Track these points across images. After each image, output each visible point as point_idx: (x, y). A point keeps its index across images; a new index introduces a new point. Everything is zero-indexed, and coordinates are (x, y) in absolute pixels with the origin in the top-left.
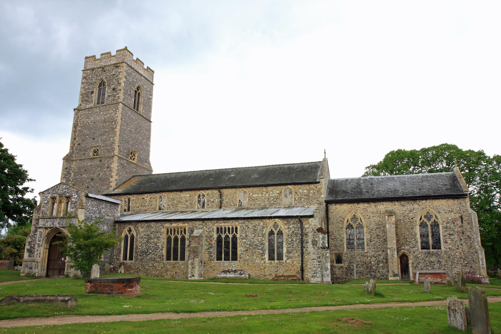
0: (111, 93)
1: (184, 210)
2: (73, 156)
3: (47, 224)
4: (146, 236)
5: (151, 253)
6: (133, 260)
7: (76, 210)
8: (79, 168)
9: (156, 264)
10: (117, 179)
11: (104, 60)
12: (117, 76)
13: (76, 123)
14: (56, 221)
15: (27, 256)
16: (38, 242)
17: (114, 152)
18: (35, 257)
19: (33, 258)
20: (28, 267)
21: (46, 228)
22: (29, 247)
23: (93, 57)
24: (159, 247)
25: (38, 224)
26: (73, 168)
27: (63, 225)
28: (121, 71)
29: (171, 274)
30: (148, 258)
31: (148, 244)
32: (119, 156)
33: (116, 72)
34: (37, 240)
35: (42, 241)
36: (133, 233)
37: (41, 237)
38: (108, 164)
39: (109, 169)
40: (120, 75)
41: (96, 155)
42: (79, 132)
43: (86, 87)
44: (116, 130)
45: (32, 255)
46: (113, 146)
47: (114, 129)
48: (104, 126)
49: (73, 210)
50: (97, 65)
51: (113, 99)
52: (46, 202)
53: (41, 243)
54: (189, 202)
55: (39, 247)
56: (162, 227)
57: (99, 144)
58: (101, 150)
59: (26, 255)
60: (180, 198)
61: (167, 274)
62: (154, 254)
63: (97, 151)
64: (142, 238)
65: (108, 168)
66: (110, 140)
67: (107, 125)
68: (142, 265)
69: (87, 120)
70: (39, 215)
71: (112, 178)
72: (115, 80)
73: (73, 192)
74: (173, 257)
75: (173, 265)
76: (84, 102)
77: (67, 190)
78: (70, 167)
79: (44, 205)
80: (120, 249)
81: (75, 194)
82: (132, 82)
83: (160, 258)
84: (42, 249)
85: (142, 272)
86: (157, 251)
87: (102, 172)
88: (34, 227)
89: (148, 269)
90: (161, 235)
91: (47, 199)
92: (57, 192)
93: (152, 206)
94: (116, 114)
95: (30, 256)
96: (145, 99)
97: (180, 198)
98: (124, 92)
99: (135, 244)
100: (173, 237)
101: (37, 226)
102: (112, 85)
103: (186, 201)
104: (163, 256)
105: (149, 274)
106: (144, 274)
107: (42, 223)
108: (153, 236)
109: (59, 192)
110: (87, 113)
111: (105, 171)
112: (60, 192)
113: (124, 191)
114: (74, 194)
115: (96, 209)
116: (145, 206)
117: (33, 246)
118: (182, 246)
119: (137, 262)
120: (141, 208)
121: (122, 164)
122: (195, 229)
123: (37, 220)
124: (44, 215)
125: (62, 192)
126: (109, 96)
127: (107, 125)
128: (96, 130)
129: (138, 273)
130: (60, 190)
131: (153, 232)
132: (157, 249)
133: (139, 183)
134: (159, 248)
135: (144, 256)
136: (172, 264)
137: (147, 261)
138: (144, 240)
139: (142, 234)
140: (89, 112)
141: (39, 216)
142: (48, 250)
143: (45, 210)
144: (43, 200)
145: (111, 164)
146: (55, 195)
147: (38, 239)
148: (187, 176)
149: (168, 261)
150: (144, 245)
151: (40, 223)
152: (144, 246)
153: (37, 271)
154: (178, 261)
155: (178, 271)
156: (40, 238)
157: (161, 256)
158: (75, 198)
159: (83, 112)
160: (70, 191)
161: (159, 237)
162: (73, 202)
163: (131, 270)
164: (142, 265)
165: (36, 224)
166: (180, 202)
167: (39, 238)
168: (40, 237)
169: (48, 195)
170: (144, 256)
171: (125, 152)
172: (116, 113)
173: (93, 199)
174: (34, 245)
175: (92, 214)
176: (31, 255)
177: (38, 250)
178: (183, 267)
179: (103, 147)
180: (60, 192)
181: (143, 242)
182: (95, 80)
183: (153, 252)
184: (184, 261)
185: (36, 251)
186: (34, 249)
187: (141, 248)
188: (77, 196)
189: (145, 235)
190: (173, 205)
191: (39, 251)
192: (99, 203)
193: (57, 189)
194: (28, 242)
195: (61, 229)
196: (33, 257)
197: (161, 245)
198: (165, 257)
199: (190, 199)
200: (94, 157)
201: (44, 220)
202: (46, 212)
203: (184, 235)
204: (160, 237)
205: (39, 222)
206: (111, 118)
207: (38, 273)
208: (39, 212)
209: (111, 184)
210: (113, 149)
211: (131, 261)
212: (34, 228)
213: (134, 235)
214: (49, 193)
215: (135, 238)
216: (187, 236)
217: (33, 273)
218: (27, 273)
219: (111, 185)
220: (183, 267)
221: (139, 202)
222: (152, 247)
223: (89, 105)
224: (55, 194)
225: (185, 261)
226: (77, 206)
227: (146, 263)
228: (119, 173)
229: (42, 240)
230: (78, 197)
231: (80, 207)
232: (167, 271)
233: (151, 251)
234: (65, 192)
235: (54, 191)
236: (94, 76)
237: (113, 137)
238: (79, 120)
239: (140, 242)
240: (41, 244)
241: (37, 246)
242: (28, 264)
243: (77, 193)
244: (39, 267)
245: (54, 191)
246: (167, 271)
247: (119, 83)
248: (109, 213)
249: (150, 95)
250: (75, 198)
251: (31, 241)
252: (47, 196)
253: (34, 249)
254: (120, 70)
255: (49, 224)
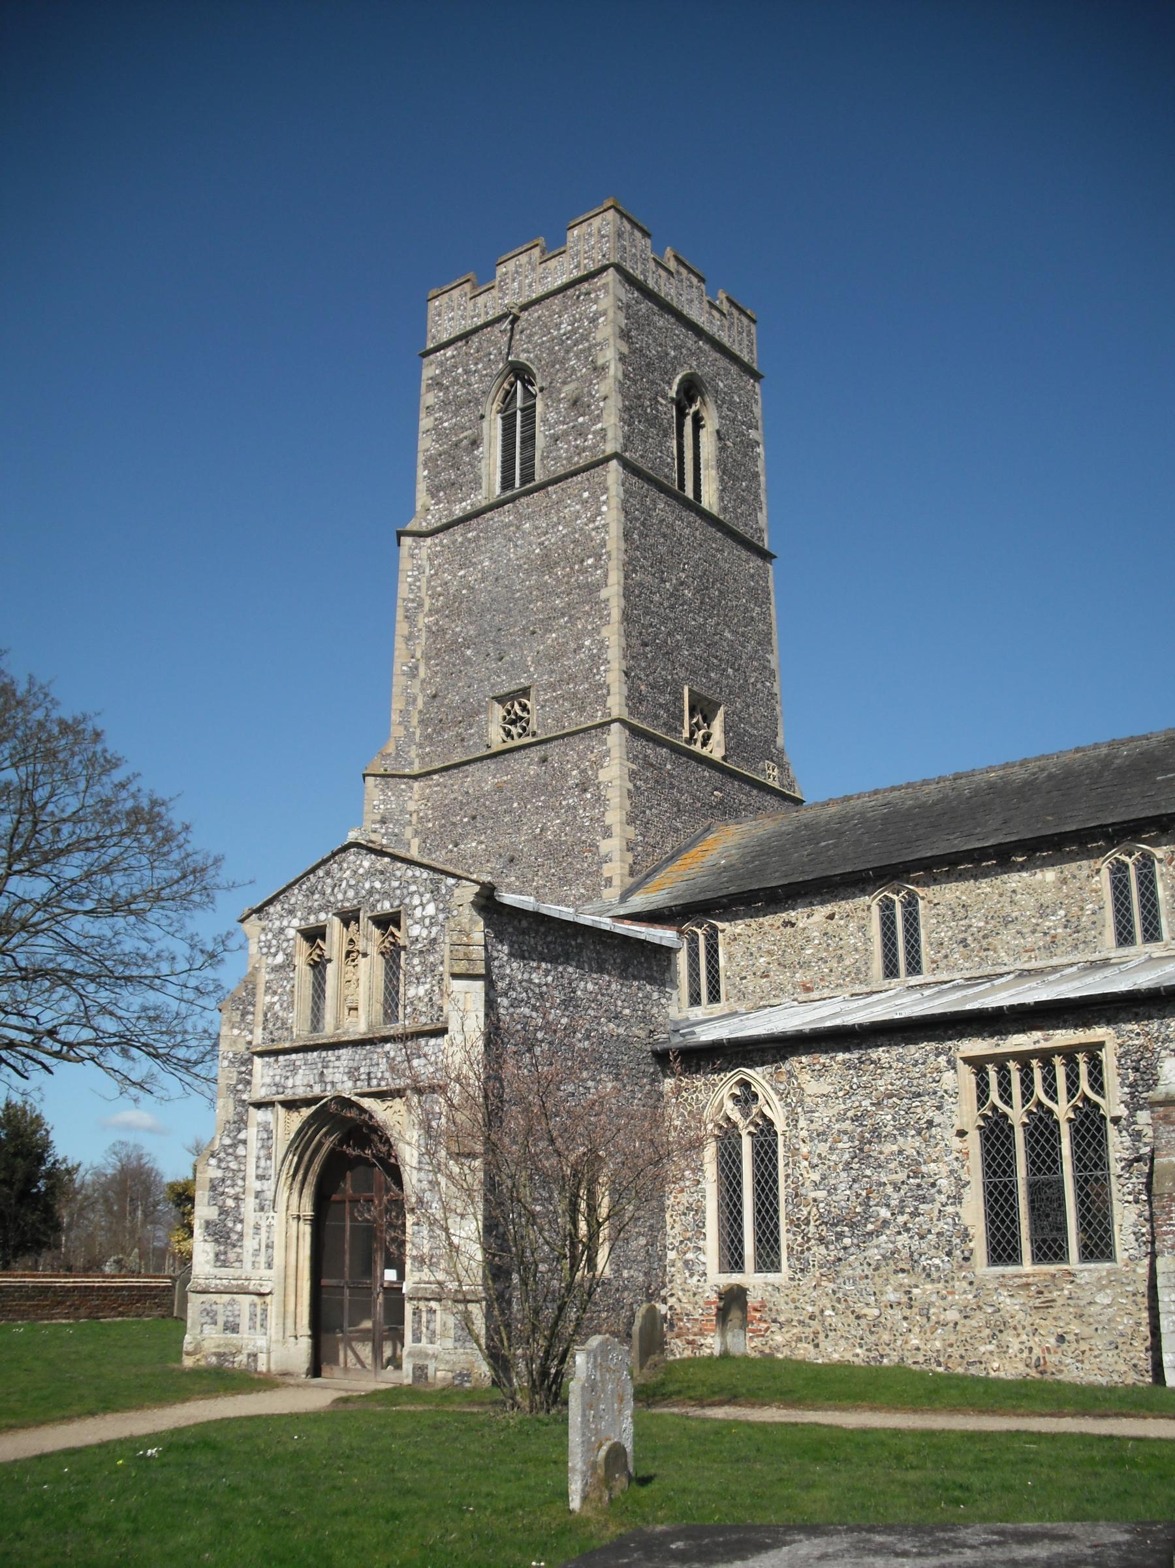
0: (564, 423)
1: (1033, 965)
2: (413, 754)
3: (290, 1083)
4: (847, 1125)
5: (885, 1223)
6: (777, 1269)
7: (436, 988)
8: (445, 811)
9: (924, 1291)
10: (637, 844)
11: (514, 280)
12: (585, 338)
13: (411, 596)
14: (338, 1059)
15: (207, 1262)
16: (258, 1185)
17: (608, 705)
18: (248, 1265)
19: (238, 1273)
20: (215, 1323)
21: (291, 1105)
22: (212, 1213)
23: (465, 285)
24: (933, 1185)
25: (249, 1083)
26: (415, 815)
27: (374, 1082)
28: (601, 309)
29: (1031, 1349)
30: (874, 1254)
31: (868, 1172)
32: (635, 722)
33: (575, 321)
34: (251, 1171)
35: (273, 1179)
36: (767, 1111)
37: (269, 1158)
38: (584, 771)
39: (589, 796)
40: (596, 327)
41: (520, 735)
42: (427, 639)
43: (446, 424)
44: (604, 594)
45: (232, 1256)
46: (598, 673)
47: (592, 589)
48: (546, 582)
49: (421, 991)
50: (487, 313)
51: (577, 447)
52: (280, 958)
53: (268, 1186)
54: (1062, 913)
55: (262, 1209)
56: (942, 1059)
57: (530, 677)
58: (542, 707)
59: (202, 1250)
60: (1005, 899)
61: (1003, 1349)
62: (908, 1230)
63: (520, 713)
64: (821, 1135)
65: (585, 790)
66: (582, 646)
67: (558, 580)
68: (839, 1300)
69: (462, 573)
70: (251, 1032)
71: (610, 837)
72: (577, 357)
73: (413, 888)
74: (1033, 1241)
75: (1041, 1293)
76: (441, 494)
77: (383, 883)
78: (403, 811)
79: (272, 976)
80: (699, 1210)
81: (421, 896)
82: (661, 359)
83: (949, 1254)
84: (278, 1219)
85: (842, 1342)
86: (923, 1207)
87: (558, 817)
88: (231, 1101)
89: (876, 1324)
90: (939, 1108)
91: (285, 945)
92: (332, 899)
93: (840, 958)
94: (600, 514)
95: (220, 1260)
96: (729, 443)
97: (1001, 895)
98: (624, 406)
99: (787, 1176)
100: (1017, 1115)
101: (245, 1097)
102: (564, 383)
103: (1043, 911)
104: (963, 1241)
105: (887, 1351)
106: (858, 1351)
107: (268, 1080)
108: (889, 1117)
109: (340, 896)
110: (460, 540)
111: (569, 808)
112: (346, 899)
113: (676, 898)
114: (416, 901)
115: (550, 979)
116: (804, 965)
117: (230, 1203)
118: (1039, 1170)
119: (808, 1281)
120: (782, 977)
121: (652, 765)
122: (1163, 1053)
123: (243, 1064)
124: (277, 1034)
125: (357, 894)
126: (556, 439)
127: (558, 580)
128: (508, 612)
129: (817, 1346)
130: (344, 884)
131: (890, 1096)
132: (923, 1199)
133: (746, 850)
134: (939, 1192)
135: (847, 1241)
136: (1028, 1285)
137: (869, 1271)
138: (840, 1145)
139: (824, 1115)
140: (470, 535)
141: (250, 1043)
142: (306, 1229)
143: (277, 1007)
144: (265, 950)
145: (598, 765)
146: (322, 916)
147: (258, 1167)
148: (1006, 783)
149: (999, 1270)
150: (844, 1175)
151: (257, 1080)
152: (842, 1186)
153: (261, 1342)
154: (1065, 1267)
155: (1075, 1328)
156: (262, 1163)
157: (956, 1241)
158: (424, 918)
159: (441, 541)
160: (396, 884)
161: (930, 1123)
162: (419, 946)
163: (775, 1327)
164: (839, 1300)
165: (240, 1087)
166: (1007, 922)
167: (259, 1158)
168: (263, 1153)
169: (285, 923)
170: (847, 1241)
171: (661, 705)
172: (599, 508)
173: (524, 924)
174: (237, 1198)
175: (526, 1011)
176: (225, 1253)
177: (257, 1228)
178: (1102, 1299)
179: (552, 687)
180: (346, 899)
181: (834, 1157)
182: (481, 381)
183: (901, 1219)
184: (1107, 1265)
185: (249, 1231)
186: (241, 1221)
187: (821, 1194)
188: (437, 908)
189: (841, 1118)
190: (964, 940)
191: (263, 1230)
192: (562, 945)
193: (329, 881)
194: (208, 1185)
195: (366, 1103)
196: (237, 1264)
197: (944, 1170)
198: (979, 1245)
199: (1067, 896)
200: (511, 744)
201: (276, 1061)
202: (280, 1014)
203: (1095, 1097)
204: (936, 1121)
205: (250, 1073)
206: (575, 541)
207: (269, 1353)
208: (250, 1017)
209: (607, 870)
210: (600, 691)
211: (772, 1277)
212: (231, 1108)
213: (772, 1124)
214: (291, 912)
215: (780, 1139)
216: (1113, 1103)
217: (245, 1352)
218: (218, 1355)
219: (606, 874)
220: (1107, 1301)
221: (766, 947)
222: (889, 1189)
223: (464, 504)
224: (322, 909)
225: (1120, 1265)
226: (442, 963)
227: (862, 1284)
228: (644, 812)
229: (272, 1172)
230: (443, 910)
231: (457, 970)
232: (998, 1329)
233: (885, 1213)
234: (371, 892)
235: (313, 893)
236: (476, 364)
237: (597, 630)
238: (424, 579)
239: (815, 1161)
240: (269, 1195)
241: (250, 1203)
242: (216, 1303)
243: (435, 891)
244: (273, 1321)
245: (316, 896)
246: (998, 1329)
247: (595, 369)
248: (619, 1003)
249: (750, 427)
250: (427, 922)
251: (223, 1180)
252: (282, 930)
253: (241, 1221)
254: (594, 307)
255: (301, 1083)
